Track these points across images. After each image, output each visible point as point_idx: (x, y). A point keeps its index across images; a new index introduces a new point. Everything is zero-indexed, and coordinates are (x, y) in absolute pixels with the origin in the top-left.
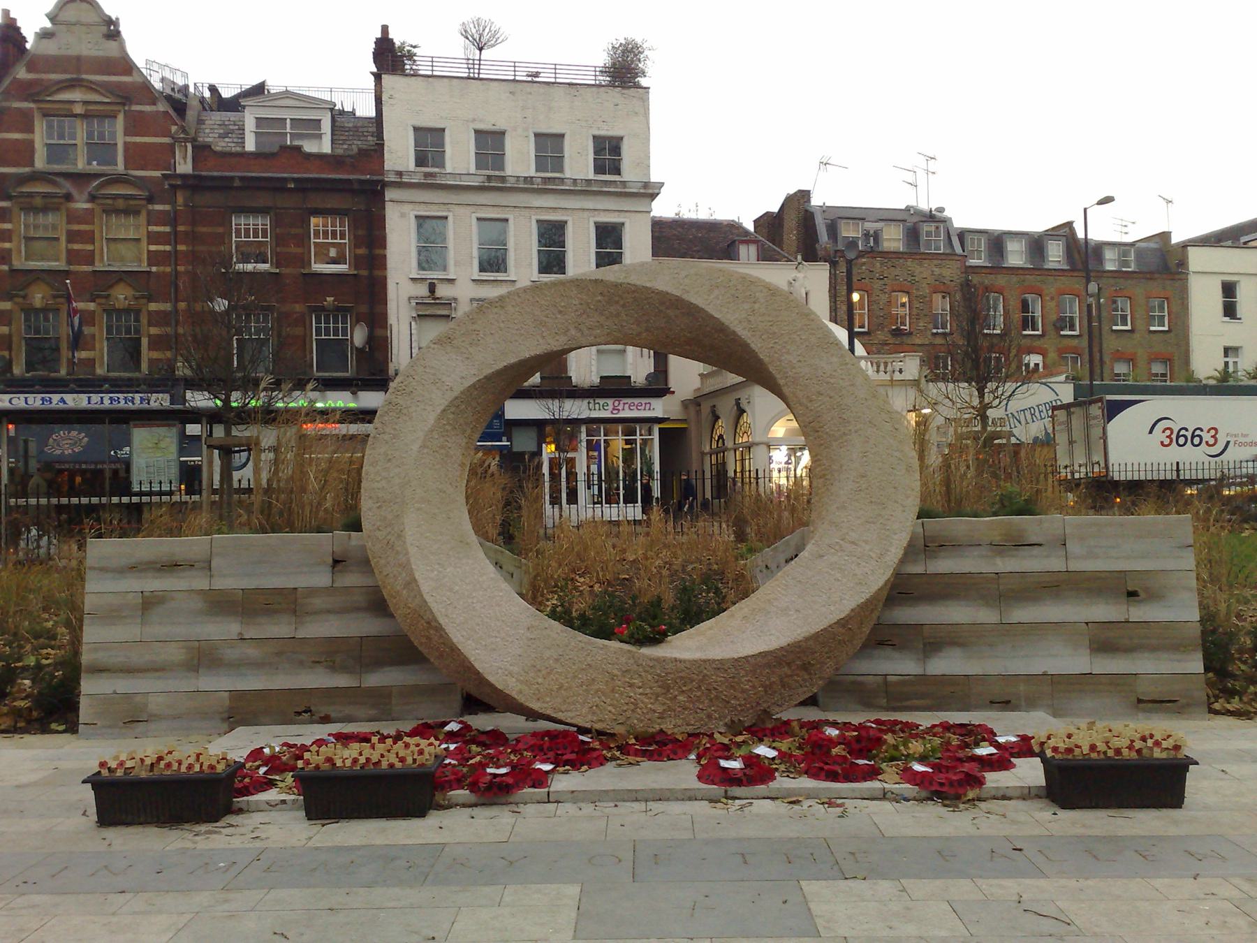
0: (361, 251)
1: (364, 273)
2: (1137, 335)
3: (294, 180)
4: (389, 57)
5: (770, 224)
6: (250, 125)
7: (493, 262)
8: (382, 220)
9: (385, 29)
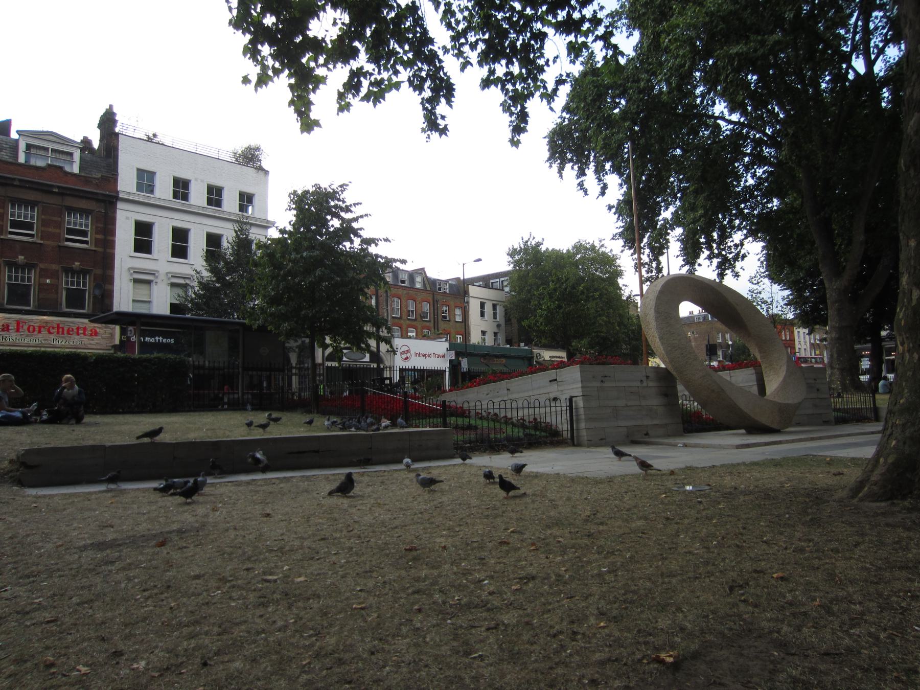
0: (99, 236)
1: (100, 250)
2: (451, 323)
3: (59, 187)
8: (113, 220)
9: (111, 106)
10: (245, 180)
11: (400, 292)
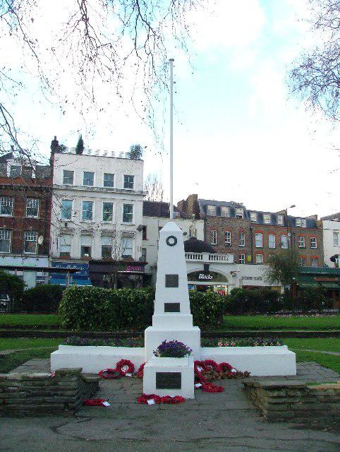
2: (307, 250)
4: (56, 147)
5: (184, 204)
6: (9, 169)
7: (89, 215)
10: (130, 168)
11: (261, 228)
